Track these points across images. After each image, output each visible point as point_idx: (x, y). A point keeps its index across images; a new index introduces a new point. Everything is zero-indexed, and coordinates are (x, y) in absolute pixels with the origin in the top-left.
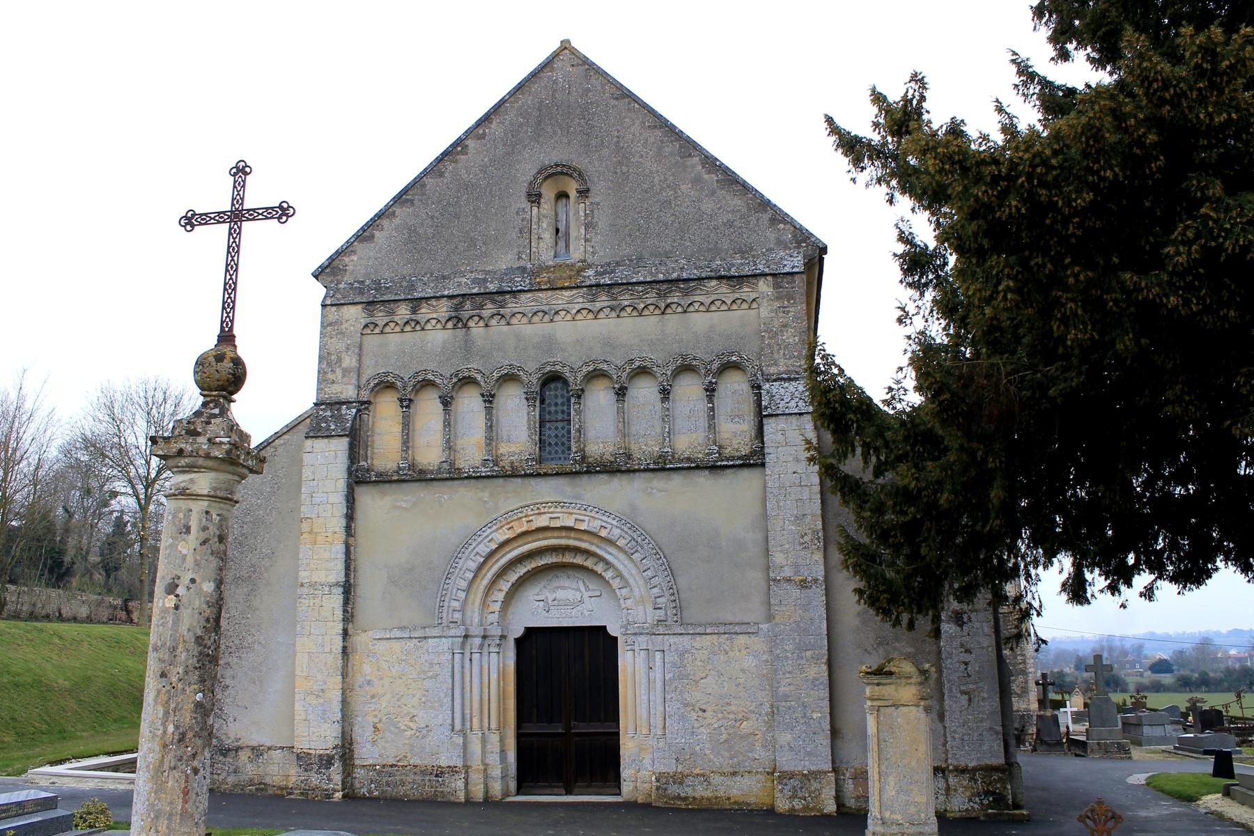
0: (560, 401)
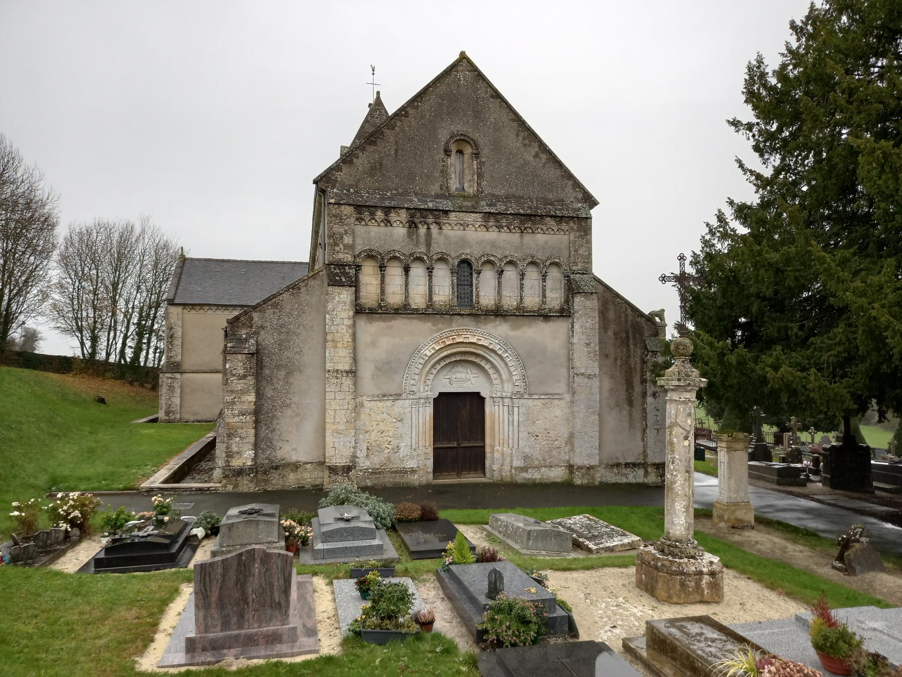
0: (466, 274)
